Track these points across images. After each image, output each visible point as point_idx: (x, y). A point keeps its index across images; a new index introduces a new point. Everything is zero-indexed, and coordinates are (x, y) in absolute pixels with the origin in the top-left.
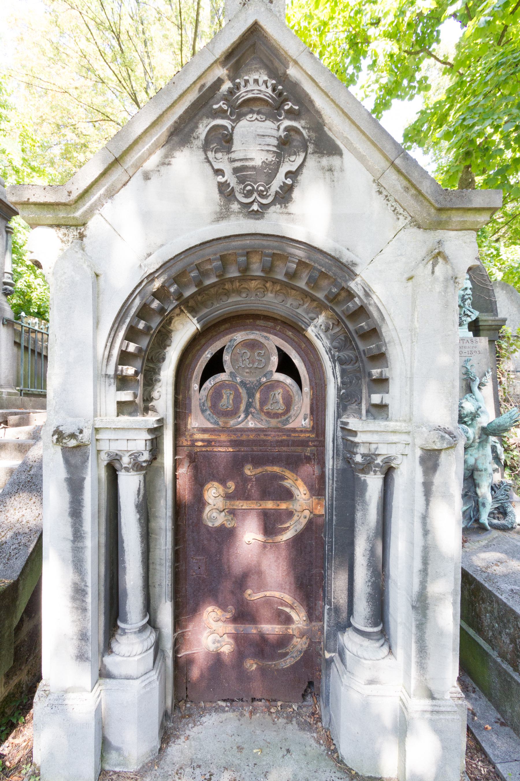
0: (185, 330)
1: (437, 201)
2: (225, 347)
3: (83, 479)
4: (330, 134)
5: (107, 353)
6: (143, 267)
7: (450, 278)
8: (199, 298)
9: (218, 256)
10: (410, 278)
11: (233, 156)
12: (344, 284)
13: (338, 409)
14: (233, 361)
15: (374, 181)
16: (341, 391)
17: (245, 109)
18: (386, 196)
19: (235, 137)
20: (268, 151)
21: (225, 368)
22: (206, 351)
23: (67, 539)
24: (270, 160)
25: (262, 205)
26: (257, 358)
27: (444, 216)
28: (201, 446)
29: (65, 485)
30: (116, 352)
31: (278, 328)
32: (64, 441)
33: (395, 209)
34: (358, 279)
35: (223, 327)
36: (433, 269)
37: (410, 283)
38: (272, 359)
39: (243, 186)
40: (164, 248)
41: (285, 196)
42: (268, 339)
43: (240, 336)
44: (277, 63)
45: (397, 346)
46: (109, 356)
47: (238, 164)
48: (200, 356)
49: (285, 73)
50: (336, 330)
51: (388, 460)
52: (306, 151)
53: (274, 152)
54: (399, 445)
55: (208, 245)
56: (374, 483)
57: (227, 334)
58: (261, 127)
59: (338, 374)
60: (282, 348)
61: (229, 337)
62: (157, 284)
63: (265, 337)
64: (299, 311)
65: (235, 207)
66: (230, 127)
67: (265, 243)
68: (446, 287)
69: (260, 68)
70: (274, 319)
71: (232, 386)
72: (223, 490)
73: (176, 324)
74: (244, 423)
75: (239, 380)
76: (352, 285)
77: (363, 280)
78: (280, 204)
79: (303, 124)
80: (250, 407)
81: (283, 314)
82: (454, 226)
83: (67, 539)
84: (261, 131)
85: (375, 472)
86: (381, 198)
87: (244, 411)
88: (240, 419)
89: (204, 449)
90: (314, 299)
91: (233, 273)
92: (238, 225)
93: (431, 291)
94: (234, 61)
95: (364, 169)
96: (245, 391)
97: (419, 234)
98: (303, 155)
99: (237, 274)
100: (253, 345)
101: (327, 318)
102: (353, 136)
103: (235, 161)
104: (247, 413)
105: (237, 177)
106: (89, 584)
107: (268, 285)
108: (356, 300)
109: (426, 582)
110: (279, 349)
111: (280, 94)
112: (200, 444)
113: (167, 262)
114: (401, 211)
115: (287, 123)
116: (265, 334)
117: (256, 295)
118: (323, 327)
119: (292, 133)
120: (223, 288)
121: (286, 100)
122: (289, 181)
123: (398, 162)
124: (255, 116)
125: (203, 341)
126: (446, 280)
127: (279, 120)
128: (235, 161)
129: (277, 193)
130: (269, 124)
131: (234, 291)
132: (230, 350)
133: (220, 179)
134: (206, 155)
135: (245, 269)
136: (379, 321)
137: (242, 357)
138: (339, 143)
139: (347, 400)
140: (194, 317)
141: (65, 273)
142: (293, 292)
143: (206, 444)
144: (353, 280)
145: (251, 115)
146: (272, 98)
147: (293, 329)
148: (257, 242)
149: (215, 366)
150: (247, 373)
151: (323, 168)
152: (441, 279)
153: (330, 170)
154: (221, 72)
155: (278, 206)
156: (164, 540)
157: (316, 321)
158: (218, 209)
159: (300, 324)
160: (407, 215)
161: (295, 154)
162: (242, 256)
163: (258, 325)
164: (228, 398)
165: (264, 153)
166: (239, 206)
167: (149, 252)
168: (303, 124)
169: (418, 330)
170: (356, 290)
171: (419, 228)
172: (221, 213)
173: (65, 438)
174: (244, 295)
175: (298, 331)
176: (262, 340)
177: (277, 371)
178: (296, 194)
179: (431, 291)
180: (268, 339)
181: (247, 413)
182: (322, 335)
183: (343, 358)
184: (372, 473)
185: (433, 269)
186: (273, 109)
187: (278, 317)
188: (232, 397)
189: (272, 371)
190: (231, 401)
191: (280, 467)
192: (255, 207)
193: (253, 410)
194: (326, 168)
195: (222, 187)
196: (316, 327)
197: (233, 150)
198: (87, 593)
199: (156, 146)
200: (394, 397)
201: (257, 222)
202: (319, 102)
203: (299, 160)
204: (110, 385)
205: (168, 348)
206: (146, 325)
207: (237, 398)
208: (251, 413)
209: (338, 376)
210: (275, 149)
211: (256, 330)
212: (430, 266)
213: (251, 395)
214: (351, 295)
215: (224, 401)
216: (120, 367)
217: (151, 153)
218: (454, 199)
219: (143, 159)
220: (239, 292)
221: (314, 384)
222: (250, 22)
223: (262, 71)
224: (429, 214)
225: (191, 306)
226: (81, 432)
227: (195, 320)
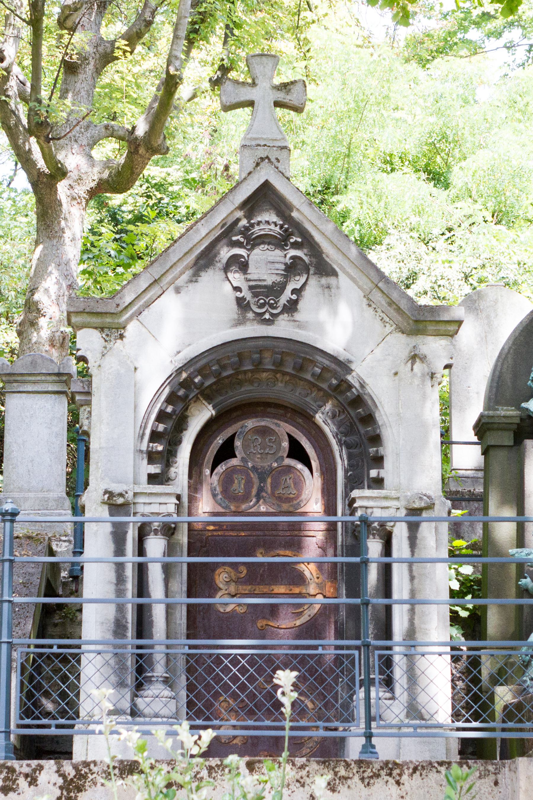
0: (201, 416)
1: (412, 315)
2: (236, 433)
3: (126, 532)
4: (328, 260)
5: (141, 432)
6: (173, 362)
7: (426, 374)
8: (214, 387)
9: (236, 353)
10: (396, 374)
11: (249, 277)
12: (342, 377)
13: (345, 490)
14: (245, 447)
15: (364, 296)
16: (348, 472)
17: (259, 241)
18: (375, 308)
19: (250, 262)
20: (277, 274)
21: (237, 453)
22: (217, 437)
23: (112, 583)
24: (278, 280)
25: (272, 315)
26: (268, 444)
27: (421, 326)
28: (213, 530)
29: (110, 537)
30: (148, 432)
31: (289, 415)
32: (114, 499)
33: (383, 318)
34: (354, 374)
35: (235, 414)
36: (412, 367)
37: (397, 377)
38: (283, 444)
39: (257, 299)
40: (191, 347)
41: (292, 307)
42: (279, 426)
43: (251, 423)
44: (283, 207)
45: (388, 429)
46: (143, 434)
47: (252, 283)
48: (211, 443)
49: (290, 215)
50: (343, 417)
51: (382, 524)
52: (308, 273)
53: (282, 275)
54: (391, 510)
55: (228, 345)
56: (374, 547)
57: (239, 421)
58: (271, 256)
59: (345, 457)
60: (293, 434)
61: (240, 424)
62: (184, 375)
63: (276, 424)
64: (308, 399)
65: (250, 315)
66: (246, 256)
67: (275, 343)
68: (423, 381)
69: (270, 209)
70: (285, 408)
71: (242, 470)
72: (235, 575)
73: (192, 410)
74: (256, 507)
75: (250, 465)
76: (349, 378)
77: (358, 374)
78: (287, 313)
79: (306, 252)
80: (262, 492)
81: (292, 402)
82: (431, 332)
83: (112, 583)
84: (271, 259)
85: (374, 535)
86: (371, 310)
87: (256, 496)
88: (252, 503)
89: (215, 533)
90: (320, 389)
91: (248, 367)
92: (252, 330)
93: (411, 384)
94: (249, 206)
95: (356, 287)
96: (257, 476)
97: (402, 338)
98: (305, 276)
99: (250, 367)
100: (264, 432)
101: (334, 406)
102: (345, 264)
103: (250, 280)
104: (259, 497)
105: (252, 292)
106: (130, 620)
107: (278, 376)
108: (354, 390)
109: (414, 619)
110: (289, 436)
111: (286, 230)
112: (212, 528)
113: (193, 358)
114: (388, 320)
115: (293, 252)
116: (276, 421)
117: (268, 384)
118: (329, 414)
119: (297, 260)
120: (235, 381)
121: (292, 234)
122: (294, 297)
123: (380, 285)
124: (266, 247)
125: (215, 427)
126: (423, 375)
127: (286, 250)
128: (250, 280)
129: (284, 305)
130: (278, 252)
131: (246, 381)
132: (241, 436)
133: (238, 294)
134: (226, 275)
135: (259, 363)
136: (373, 407)
137: (253, 443)
138: (335, 267)
139: (355, 481)
140: (209, 404)
141: (112, 367)
142: (302, 383)
143: (217, 528)
144: (350, 374)
145: (263, 246)
146: (280, 234)
147: (303, 417)
148: (269, 343)
149: (227, 451)
150: (258, 458)
151: (322, 286)
152: (419, 374)
153: (329, 287)
154: (240, 214)
155: (286, 315)
156: (180, 614)
157: (323, 408)
158: (236, 316)
159: (308, 411)
160: (393, 323)
161: (299, 275)
162: (257, 353)
163: (268, 413)
164: (239, 483)
165: (274, 276)
166: (254, 315)
167: (178, 350)
168: (306, 252)
169: (402, 415)
170: (353, 382)
171: (403, 333)
172: (239, 320)
173: (115, 496)
174: (256, 385)
175: (308, 419)
176: (273, 427)
177: (288, 456)
178: (300, 306)
179: (411, 384)
180: (279, 426)
181: (259, 497)
182: (329, 421)
183: (350, 442)
184: (371, 537)
185: (412, 367)
186: (280, 242)
187: (288, 405)
188: (243, 481)
189: (283, 457)
190: (242, 486)
191: (292, 551)
192: (267, 316)
193: (264, 494)
194: (325, 286)
195: (240, 301)
196: (323, 413)
197: (249, 272)
198: (127, 629)
199: (186, 268)
200: (388, 472)
201: (269, 327)
202: (318, 237)
203: (303, 279)
204: (143, 459)
205: (184, 432)
206: (173, 409)
207: (249, 483)
208: (263, 497)
209: (345, 459)
210: (283, 272)
211: (267, 417)
212: (409, 364)
213: (262, 480)
214: (350, 386)
215: (235, 486)
216: (151, 444)
217: (182, 273)
218: (426, 314)
219: (176, 278)
220: (251, 382)
221: (324, 469)
222: (262, 181)
223: (271, 211)
224: (409, 324)
225: (208, 394)
226: (127, 493)
227: (210, 407)
